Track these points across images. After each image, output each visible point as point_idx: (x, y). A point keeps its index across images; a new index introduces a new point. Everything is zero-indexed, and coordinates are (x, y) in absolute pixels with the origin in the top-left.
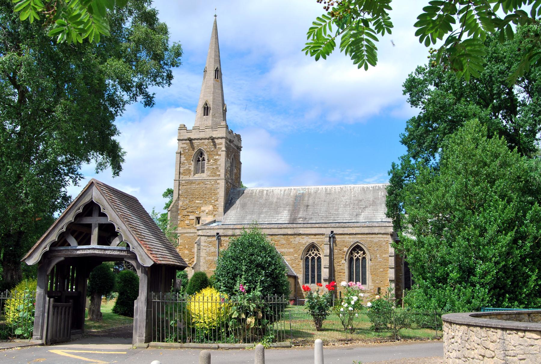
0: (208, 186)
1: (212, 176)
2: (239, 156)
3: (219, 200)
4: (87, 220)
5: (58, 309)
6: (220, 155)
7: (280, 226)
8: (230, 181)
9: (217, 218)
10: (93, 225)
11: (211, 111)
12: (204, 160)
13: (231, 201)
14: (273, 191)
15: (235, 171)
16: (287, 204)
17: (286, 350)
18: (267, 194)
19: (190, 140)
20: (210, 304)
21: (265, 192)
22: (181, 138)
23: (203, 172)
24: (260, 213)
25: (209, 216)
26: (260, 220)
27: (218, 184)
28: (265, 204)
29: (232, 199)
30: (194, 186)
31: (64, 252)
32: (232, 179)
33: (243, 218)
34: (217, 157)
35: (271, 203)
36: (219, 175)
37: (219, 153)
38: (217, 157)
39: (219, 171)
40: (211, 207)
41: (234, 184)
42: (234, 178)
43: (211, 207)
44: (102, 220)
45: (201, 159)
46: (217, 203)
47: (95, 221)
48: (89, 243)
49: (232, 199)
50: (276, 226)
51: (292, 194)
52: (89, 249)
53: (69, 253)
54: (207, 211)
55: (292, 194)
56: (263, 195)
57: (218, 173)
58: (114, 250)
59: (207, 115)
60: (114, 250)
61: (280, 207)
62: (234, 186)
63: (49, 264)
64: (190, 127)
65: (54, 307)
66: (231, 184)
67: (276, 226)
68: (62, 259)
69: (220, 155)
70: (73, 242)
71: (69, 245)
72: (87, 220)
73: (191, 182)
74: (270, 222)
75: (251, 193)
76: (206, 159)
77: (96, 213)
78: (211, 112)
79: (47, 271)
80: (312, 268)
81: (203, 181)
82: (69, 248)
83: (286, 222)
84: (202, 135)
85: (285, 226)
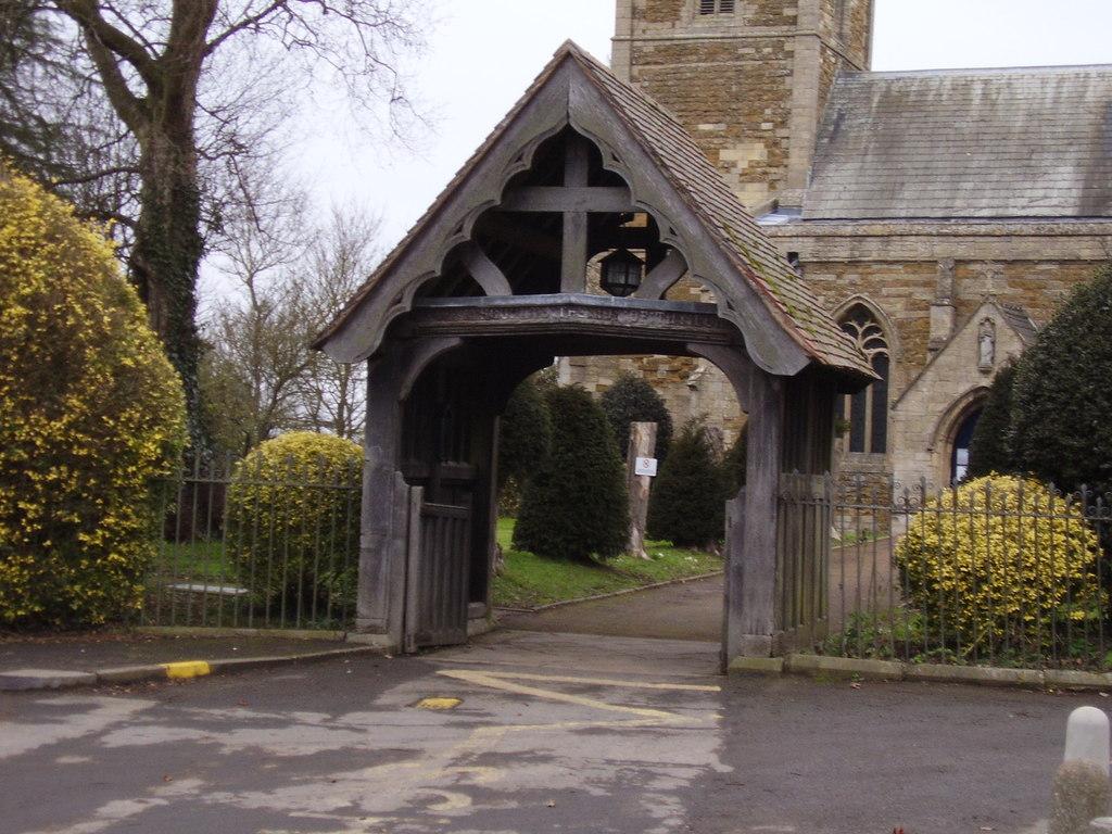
0: (748, 65)
1: (766, 23)
3: (795, 121)
4: (548, 201)
5: (435, 525)
7: (1047, 226)
8: (833, 42)
9: (788, 196)
10: (567, 218)
13: (837, 125)
14: (1009, 85)
16: (1072, 139)
18: (985, 95)
21: (978, 89)
24: (957, 177)
25: (749, 186)
26: (958, 203)
27: (791, 54)
28: (978, 137)
29: (841, 117)
30: (693, 64)
31: (461, 320)
32: (841, 36)
33: (892, 191)
35: (1005, 136)
36: (794, 21)
40: (758, 152)
41: (850, 56)
42: (847, 30)
43: (758, 152)
44: (604, 201)
46: (782, 132)
47: (575, 201)
48: (555, 289)
49: (841, 117)
50: (1030, 228)
51: (1090, 96)
52: (555, 307)
53: (482, 321)
54: (742, 165)
55: (1090, 96)
56: (967, 100)
57: (788, 12)
58: (650, 312)
60: (650, 312)
61: (1043, 149)
62: (848, 62)
63: (407, 359)
65: (426, 516)
66: (836, 54)
67: (1030, 228)
68: (454, 342)
70: (495, 285)
71: (481, 292)
72: (548, 201)
73: (678, 51)
74: (1001, 212)
75: (921, 94)
77: (576, 174)
80: (874, 434)
81: (724, 48)
82: (481, 302)
83: (1069, 212)
85: (1067, 226)
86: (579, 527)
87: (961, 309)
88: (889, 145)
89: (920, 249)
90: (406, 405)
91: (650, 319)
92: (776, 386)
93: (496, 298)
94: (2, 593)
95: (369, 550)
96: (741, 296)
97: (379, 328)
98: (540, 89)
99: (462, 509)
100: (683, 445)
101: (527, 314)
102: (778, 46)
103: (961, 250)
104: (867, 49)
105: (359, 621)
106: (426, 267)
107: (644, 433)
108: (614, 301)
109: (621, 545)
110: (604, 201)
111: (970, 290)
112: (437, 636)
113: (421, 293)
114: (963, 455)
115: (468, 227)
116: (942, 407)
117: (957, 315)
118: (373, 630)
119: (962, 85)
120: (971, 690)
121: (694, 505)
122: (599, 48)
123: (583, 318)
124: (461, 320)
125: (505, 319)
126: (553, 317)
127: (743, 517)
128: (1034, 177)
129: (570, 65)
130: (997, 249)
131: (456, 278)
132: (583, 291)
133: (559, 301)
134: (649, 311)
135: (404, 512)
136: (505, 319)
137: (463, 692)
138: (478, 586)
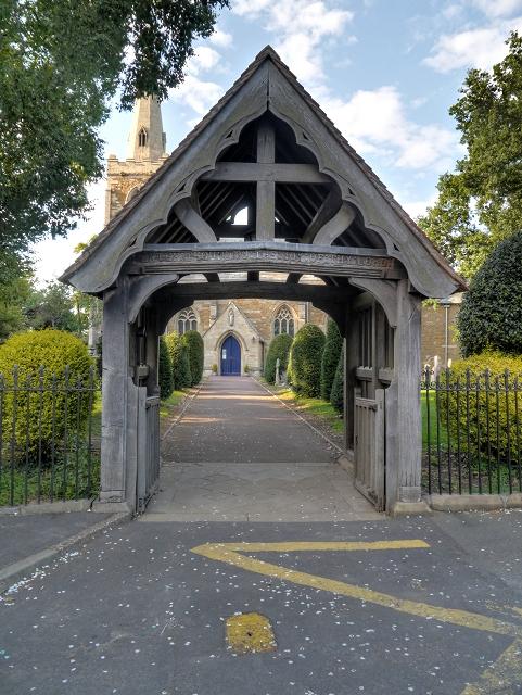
19: (124, 175)
22: (112, 172)
44: (294, 174)
47: (266, 172)
63: (133, 292)
71: (193, 240)
78: (148, 141)
79: (128, 312)
82: (195, 247)
90: (133, 326)
91: (325, 260)
93: (206, 244)
94: (193, 2)
95: (108, 439)
96: (405, 240)
97: (118, 263)
98: (237, 92)
101: (231, 256)
105: (102, 494)
106: (156, 217)
110: (294, 174)
113: (149, 240)
115: (190, 185)
117: (218, 309)
118: (112, 500)
127: (396, 402)
133: (257, 247)
134: (325, 254)
135: (136, 407)
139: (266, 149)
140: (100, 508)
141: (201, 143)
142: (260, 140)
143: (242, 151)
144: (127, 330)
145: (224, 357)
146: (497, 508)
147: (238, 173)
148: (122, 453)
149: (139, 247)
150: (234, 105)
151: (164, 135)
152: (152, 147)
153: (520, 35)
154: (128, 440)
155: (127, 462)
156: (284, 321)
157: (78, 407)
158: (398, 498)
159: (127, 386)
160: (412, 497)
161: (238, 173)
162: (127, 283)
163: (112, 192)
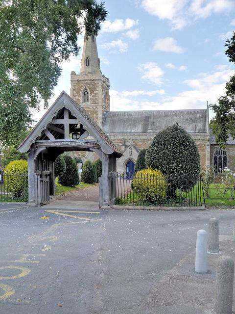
0: (91, 110)
2: (108, 91)
6: (98, 91)
10: (65, 125)
11: (91, 63)
12: (88, 94)
15: (107, 101)
17: (201, 212)
18: (128, 115)
19: (78, 81)
20: (149, 181)
22: (73, 80)
23: (88, 101)
31: (45, 144)
34: (96, 92)
37: (97, 89)
38: (96, 92)
39: (98, 101)
44: (73, 121)
45: (86, 93)
47: (66, 122)
48: (64, 138)
56: (125, 116)
59: (88, 65)
63: (35, 152)
64: (78, 73)
65: (41, 181)
68: (45, 148)
69: (98, 91)
71: (49, 139)
76: (89, 93)
78: (91, 63)
79: (34, 157)
82: (49, 141)
84: (86, 78)
86: (70, 180)
87: (126, 146)
88: (114, 122)
89: (119, 137)
92: (107, 156)
99: (48, 180)
100: (220, 103)
102: (96, 107)
103: (126, 137)
104: (109, 108)
106: (38, 134)
107: (79, 165)
108: (75, 140)
109: (79, 183)
110: (73, 121)
111: (127, 143)
112: (44, 203)
113: (37, 139)
114: (127, 167)
115: (46, 126)
116: (124, 161)
117: (125, 147)
119: (124, 113)
120: (182, 211)
121: (91, 177)
122: (69, 93)
123: (69, 144)
124: (45, 144)
125: (54, 144)
126: (63, 143)
128: (136, 127)
129: (64, 96)
130: (131, 137)
131: (44, 137)
132: (68, 140)
136: (54, 144)
137: (51, 216)
138: (51, 193)
139: (66, 115)
140: (28, 204)
141: (48, 115)
142: (65, 113)
143: (61, 115)
144: (97, 159)
145: (128, 171)
146: (131, 209)
147: (59, 122)
148: (33, 191)
149: (34, 142)
150: (56, 106)
151: (99, 59)
152: (92, 66)
153: (117, 92)
154: (35, 188)
155: (35, 193)
156: (221, 151)
157: (26, 181)
158: (103, 205)
159: (34, 175)
160: (106, 205)
161: (59, 122)
162: (33, 150)
163: (73, 90)
